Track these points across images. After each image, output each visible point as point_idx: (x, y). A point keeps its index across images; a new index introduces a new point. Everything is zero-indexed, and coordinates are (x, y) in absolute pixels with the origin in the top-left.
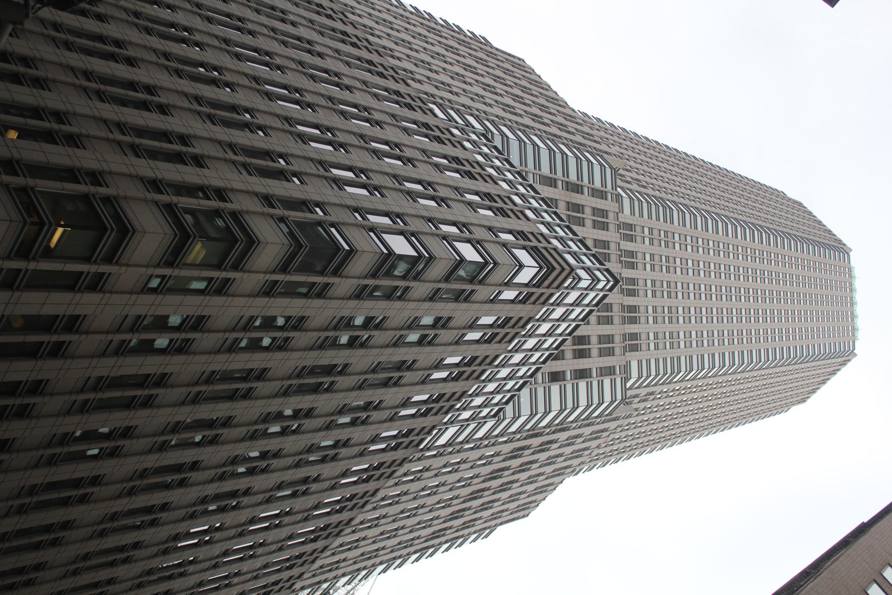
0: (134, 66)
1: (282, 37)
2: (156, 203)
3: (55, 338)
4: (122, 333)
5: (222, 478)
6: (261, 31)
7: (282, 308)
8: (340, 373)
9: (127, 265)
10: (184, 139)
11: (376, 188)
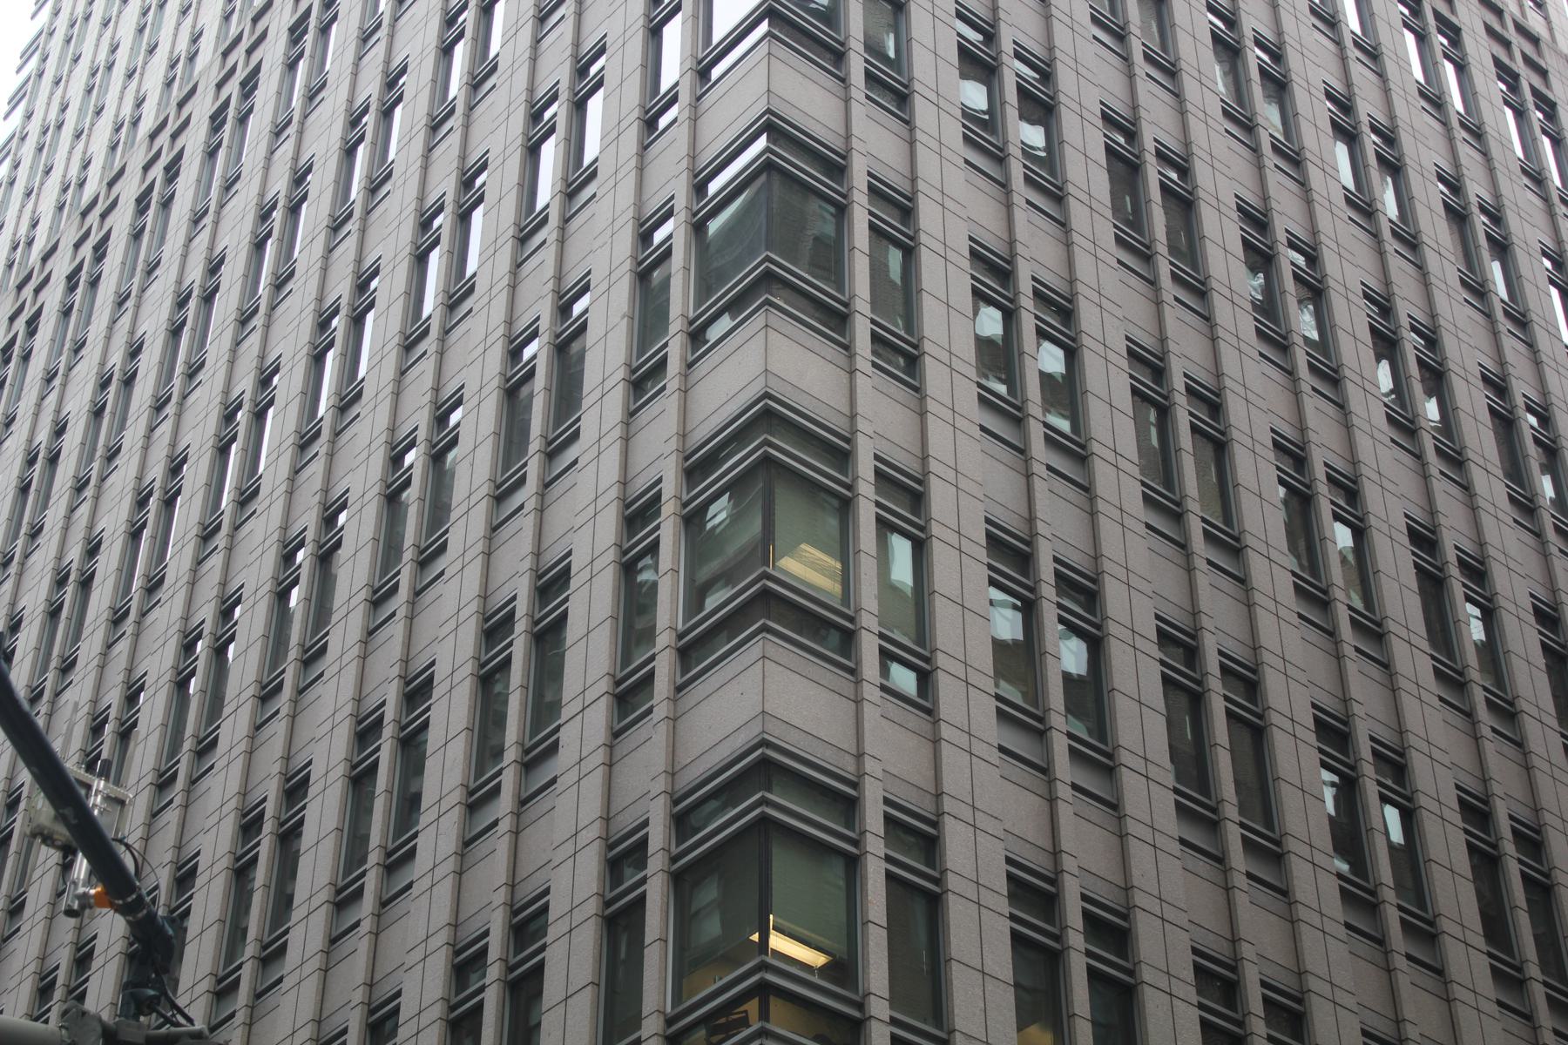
0: (307, 778)
1: (177, 381)
2: (679, 689)
3: (1076, 939)
4: (1050, 760)
5: (1456, 460)
6: (166, 439)
7: (953, 322)
8: (1132, 135)
9: (859, 756)
10: (495, 628)
11: (582, 72)
